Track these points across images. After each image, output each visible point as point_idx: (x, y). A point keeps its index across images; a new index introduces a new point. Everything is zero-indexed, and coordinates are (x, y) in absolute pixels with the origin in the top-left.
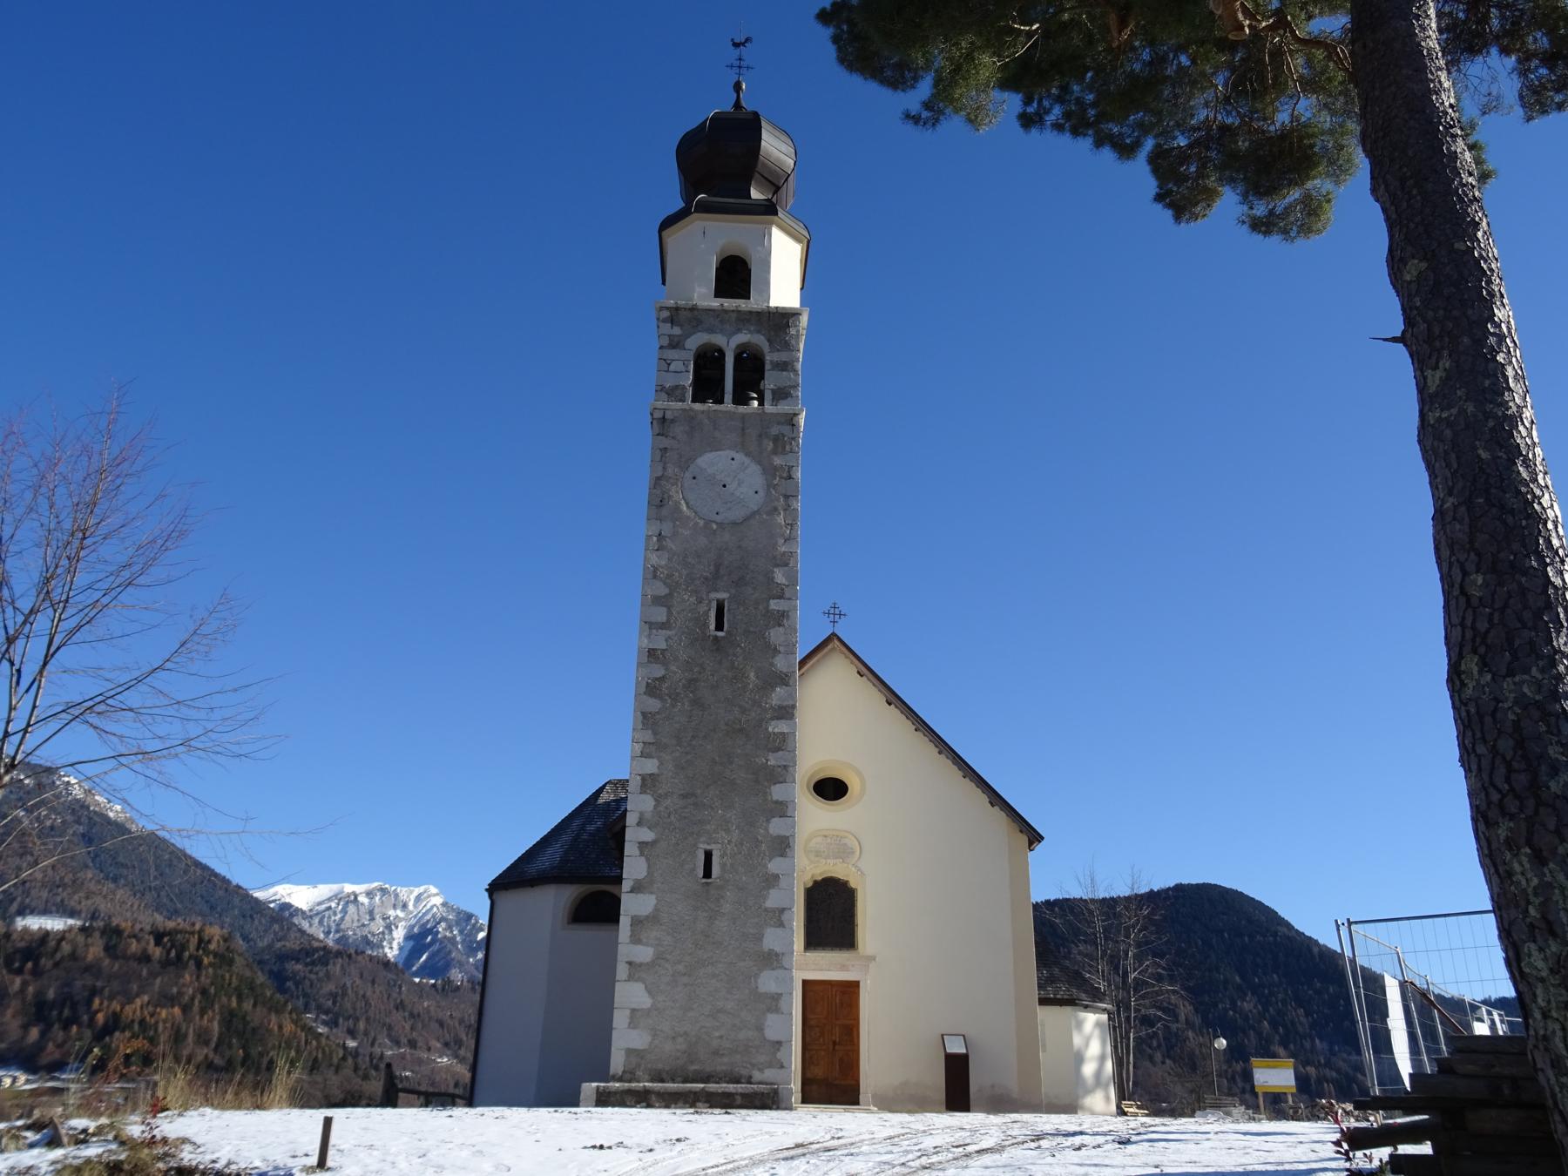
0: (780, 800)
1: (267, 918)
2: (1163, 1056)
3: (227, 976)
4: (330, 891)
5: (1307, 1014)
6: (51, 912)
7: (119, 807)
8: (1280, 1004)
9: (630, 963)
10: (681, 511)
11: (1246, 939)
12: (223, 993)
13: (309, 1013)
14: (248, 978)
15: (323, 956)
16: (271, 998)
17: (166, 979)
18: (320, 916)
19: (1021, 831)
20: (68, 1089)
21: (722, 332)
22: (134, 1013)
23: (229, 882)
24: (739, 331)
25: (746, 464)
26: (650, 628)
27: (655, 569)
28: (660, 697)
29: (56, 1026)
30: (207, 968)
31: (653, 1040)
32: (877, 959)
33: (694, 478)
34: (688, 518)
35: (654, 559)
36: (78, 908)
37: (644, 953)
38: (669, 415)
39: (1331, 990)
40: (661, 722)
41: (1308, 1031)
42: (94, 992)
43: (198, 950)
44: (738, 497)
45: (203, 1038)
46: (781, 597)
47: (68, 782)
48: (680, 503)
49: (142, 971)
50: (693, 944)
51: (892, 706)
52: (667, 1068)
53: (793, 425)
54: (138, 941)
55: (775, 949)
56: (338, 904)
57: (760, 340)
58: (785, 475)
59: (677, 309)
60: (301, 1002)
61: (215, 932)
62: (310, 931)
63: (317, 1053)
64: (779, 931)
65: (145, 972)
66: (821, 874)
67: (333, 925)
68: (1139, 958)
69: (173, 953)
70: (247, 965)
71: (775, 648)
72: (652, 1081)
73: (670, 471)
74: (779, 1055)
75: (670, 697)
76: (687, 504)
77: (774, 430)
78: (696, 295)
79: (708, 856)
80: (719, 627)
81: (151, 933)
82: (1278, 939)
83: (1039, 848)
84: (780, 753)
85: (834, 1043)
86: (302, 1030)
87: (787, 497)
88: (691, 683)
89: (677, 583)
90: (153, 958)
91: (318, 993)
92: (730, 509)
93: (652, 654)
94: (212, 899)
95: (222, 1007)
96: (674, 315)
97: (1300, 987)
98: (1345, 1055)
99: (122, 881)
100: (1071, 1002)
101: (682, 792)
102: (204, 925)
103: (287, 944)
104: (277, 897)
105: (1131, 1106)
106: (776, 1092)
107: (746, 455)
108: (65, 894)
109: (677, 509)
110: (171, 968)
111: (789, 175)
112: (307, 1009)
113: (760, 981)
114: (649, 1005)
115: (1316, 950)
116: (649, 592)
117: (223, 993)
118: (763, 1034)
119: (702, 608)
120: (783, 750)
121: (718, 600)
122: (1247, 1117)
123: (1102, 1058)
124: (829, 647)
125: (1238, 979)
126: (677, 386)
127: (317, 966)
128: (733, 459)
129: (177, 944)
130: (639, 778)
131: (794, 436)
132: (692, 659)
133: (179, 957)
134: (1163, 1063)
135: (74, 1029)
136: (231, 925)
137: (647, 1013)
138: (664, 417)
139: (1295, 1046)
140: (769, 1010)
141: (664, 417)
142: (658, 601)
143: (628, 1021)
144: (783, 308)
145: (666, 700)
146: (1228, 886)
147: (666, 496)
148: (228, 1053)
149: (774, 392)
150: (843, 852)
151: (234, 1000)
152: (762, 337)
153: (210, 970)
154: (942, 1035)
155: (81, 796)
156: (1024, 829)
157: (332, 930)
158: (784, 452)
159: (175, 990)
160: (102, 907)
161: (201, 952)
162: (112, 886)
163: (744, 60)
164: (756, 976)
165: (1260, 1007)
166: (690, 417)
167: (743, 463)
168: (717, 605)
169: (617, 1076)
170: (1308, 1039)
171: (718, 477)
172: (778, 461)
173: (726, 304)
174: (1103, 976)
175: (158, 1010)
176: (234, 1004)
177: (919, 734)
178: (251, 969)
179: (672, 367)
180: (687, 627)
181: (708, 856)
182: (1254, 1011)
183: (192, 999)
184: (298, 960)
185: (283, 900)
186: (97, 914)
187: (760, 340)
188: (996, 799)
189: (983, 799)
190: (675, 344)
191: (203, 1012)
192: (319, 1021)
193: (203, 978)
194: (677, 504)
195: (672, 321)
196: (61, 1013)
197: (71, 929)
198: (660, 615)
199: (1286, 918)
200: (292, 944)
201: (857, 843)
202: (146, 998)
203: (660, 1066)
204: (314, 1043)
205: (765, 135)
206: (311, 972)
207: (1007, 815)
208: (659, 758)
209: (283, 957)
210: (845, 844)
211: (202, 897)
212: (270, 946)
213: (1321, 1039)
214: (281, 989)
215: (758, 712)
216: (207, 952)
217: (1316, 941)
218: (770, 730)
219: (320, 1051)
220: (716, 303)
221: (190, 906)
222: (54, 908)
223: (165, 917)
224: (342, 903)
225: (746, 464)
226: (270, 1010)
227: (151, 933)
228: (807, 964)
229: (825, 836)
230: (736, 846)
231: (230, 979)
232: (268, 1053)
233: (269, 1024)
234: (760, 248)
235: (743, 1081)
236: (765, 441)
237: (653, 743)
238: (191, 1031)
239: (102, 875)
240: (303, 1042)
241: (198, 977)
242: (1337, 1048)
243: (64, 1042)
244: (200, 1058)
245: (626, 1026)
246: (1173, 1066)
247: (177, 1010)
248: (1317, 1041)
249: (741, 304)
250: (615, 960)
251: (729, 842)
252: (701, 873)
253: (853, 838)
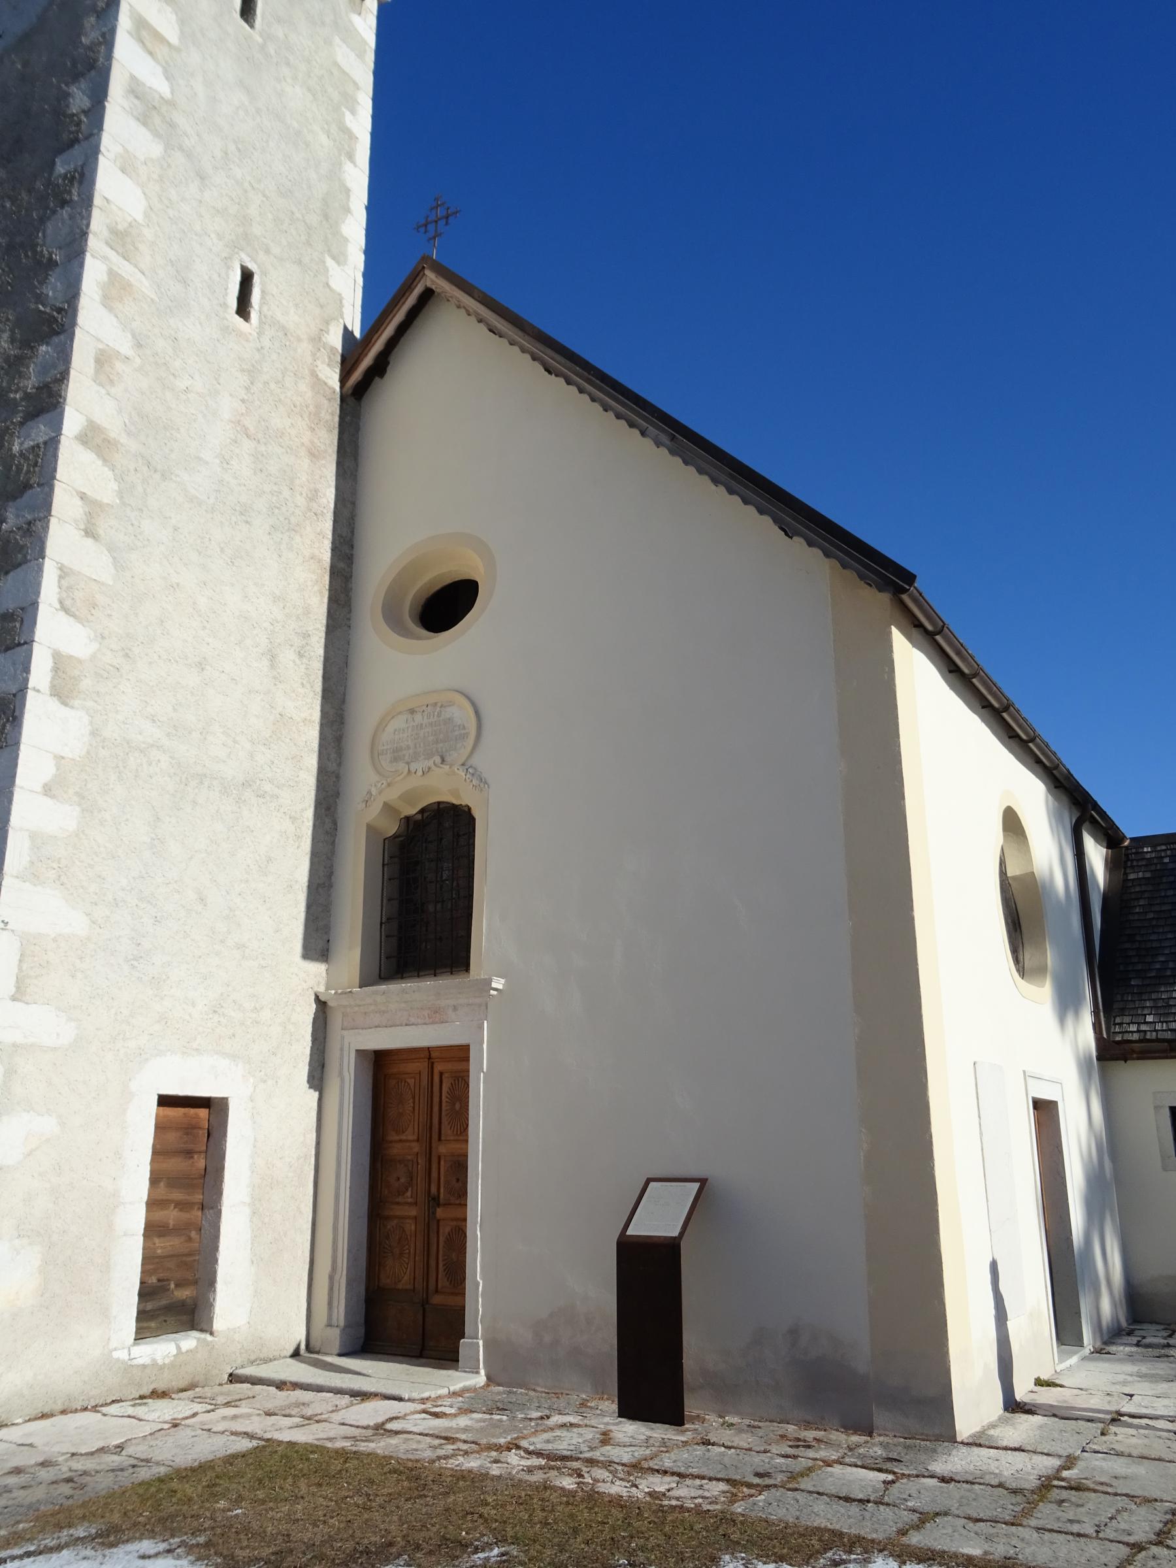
207: (827, 554)
229: (412, 711)
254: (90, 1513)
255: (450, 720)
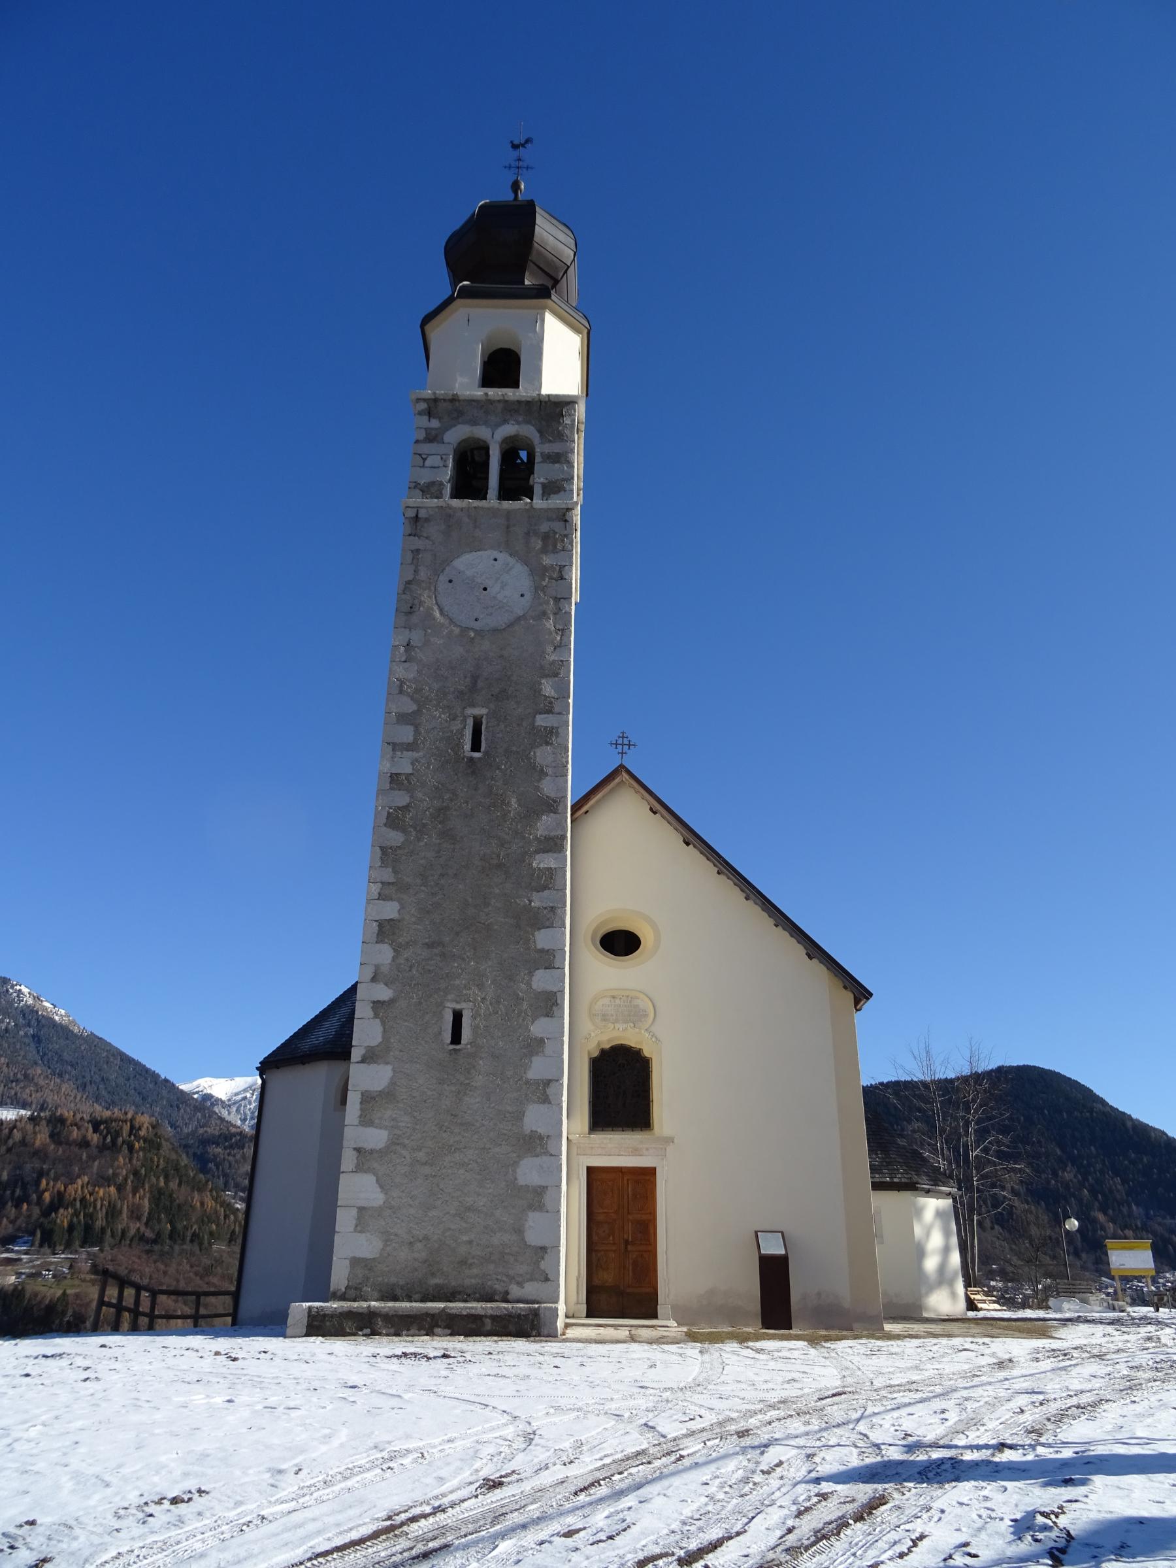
0: (546, 948)
1: (191, 1107)
2: (992, 1222)
3: (156, 1159)
4: (246, 1083)
5: (1124, 1182)
6: (6, 1104)
7: (63, 1012)
8: (1098, 1173)
9: (358, 1150)
10: (434, 619)
11: (1065, 1115)
12: (152, 1173)
13: (229, 1191)
14: (173, 1160)
15: (240, 1140)
16: (194, 1177)
17: (103, 1161)
18: (237, 1105)
19: (845, 988)
20: (20, 1260)
21: (486, 423)
22: (76, 1192)
23: (158, 1076)
24: (505, 421)
25: (511, 565)
26: (393, 750)
27: (402, 683)
28: (404, 830)
29: (10, 1204)
30: (138, 1152)
31: (385, 1245)
32: (676, 1141)
33: (450, 581)
34: (442, 625)
35: (401, 672)
36: (29, 1100)
37: (376, 1138)
38: (422, 514)
39: (1145, 1160)
40: (404, 857)
41: (1125, 1197)
42: (41, 1174)
43: (130, 1136)
44: (500, 601)
45: (135, 1214)
46: (549, 711)
47: (20, 990)
48: (433, 610)
49: (82, 1155)
50: (436, 1125)
51: (691, 846)
52: (402, 1282)
53: (566, 521)
54: (79, 1129)
55: (539, 1130)
56: (253, 1094)
57: (529, 431)
58: (555, 575)
59: (436, 400)
60: (221, 1182)
61: (145, 1120)
62: (228, 1118)
63: (235, 1224)
64: (543, 1108)
65: (84, 1156)
66: (609, 1041)
67: (248, 1113)
68: (982, 1134)
69: (109, 1139)
70: (173, 1149)
71: (542, 770)
72: (383, 1298)
73: (423, 574)
74: (543, 1265)
75: (415, 829)
76: (441, 611)
77: (544, 527)
78: (457, 385)
79: (458, 1017)
80: (476, 747)
81: (89, 1122)
82: (1094, 1114)
83: (868, 1006)
84: (547, 892)
85: (627, 1242)
86: (221, 1206)
87: (557, 600)
88: (441, 813)
89: (427, 698)
90: (92, 1144)
91: (236, 1173)
92: (491, 614)
93: (395, 780)
94: (144, 1091)
95: (151, 1187)
96: (432, 407)
97: (1116, 1158)
98: (1159, 1219)
99: (67, 1076)
100: (911, 1187)
101: (427, 940)
102: (136, 1113)
103: (208, 1130)
104: (200, 1089)
105: (978, 1293)
106: (536, 1313)
107: (511, 555)
108: (18, 1087)
109: (429, 615)
110: (107, 1153)
111: (568, 267)
112: (226, 1187)
113: (519, 1171)
114: (381, 1202)
115: (1129, 1124)
116: (394, 709)
117: (152, 1173)
118: (523, 1239)
119: (456, 726)
120: (549, 889)
121: (475, 717)
122: (1105, 1304)
123: (946, 1250)
124: (617, 780)
125: (1059, 1152)
126: (434, 482)
127: (234, 1149)
128: (496, 560)
129: (112, 1131)
130: (375, 924)
131: (565, 533)
132: (442, 785)
133: (114, 1141)
134: (992, 1228)
135: (25, 1206)
136: (161, 1114)
137: (379, 1212)
138: (417, 516)
139: (1114, 1210)
140: (531, 1207)
141: (417, 516)
142: (403, 718)
143: (354, 1222)
144: (557, 396)
145: (411, 832)
146: (1047, 1067)
147: (416, 602)
148: (157, 1228)
149: (544, 486)
150: (635, 1016)
151: (162, 1179)
152: (532, 428)
153: (141, 1154)
154: (756, 1232)
155: (30, 1002)
156: (848, 984)
157: (248, 1117)
158: (555, 551)
159: (111, 1171)
160: (49, 1100)
161: (133, 1137)
162: (58, 1080)
163: (523, 161)
164: (516, 1164)
165: (1080, 1177)
166: (447, 515)
167: (508, 565)
168: (474, 721)
169: (339, 1294)
170: (1125, 1204)
171: (479, 580)
172: (547, 560)
173: (489, 393)
174: (943, 1154)
175: (97, 1189)
176: (162, 1184)
177: (723, 878)
178: (176, 1152)
179: (428, 463)
180: (437, 748)
181: (458, 1017)
182: (1075, 1180)
183: (126, 1179)
184: (218, 1145)
185: (205, 1092)
186: (45, 1105)
187: (529, 431)
188: (815, 951)
189: (800, 950)
190: (432, 437)
191: (135, 1191)
192: (238, 1198)
193: (134, 1161)
194: (429, 612)
195: (429, 413)
196: (13, 1192)
197: (21, 1119)
198: (406, 734)
199: (1101, 1096)
200: (213, 1130)
201: (650, 1004)
202: (86, 1179)
203: (393, 1280)
204: (232, 1217)
205: (539, 220)
206: (229, 1154)
207: (828, 969)
208: (399, 900)
209: (206, 1142)
210: (638, 1006)
211: (135, 1089)
212: (194, 1132)
213: (1137, 1205)
214: (204, 1170)
215: (521, 844)
216: (138, 1138)
217: (1130, 1116)
218: (535, 865)
219: (237, 1223)
220: (479, 393)
221: (125, 1097)
222: (9, 1101)
223: (104, 1107)
224: (255, 1094)
225: (511, 565)
226: (193, 1189)
227: (89, 1122)
228: (592, 1148)
229: (614, 997)
230: (491, 1004)
231: (158, 1161)
232: (192, 1227)
233: (193, 1201)
234: (530, 335)
235: (497, 1298)
236: (533, 539)
237: (393, 883)
238: (125, 1207)
239: (49, 1071)
240: (222, 1217)
241: (130, 1160)
242: (1152, 1212)
243: (17, 1218)
244: (132, 1232)
245: (352, 1229)
246: (1001, 1231)
247: (112, 1189)
248: (1134, 1207)
249: (509, 393)
250: (340, 1147)
251: (483, 999)
252: (447, 1036)
253: (647, 999)
254: (1056, 1287)
255: (638, 1006)
